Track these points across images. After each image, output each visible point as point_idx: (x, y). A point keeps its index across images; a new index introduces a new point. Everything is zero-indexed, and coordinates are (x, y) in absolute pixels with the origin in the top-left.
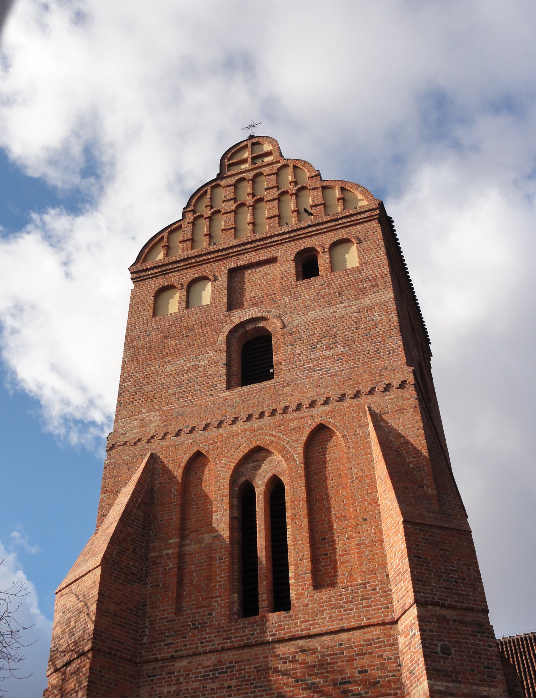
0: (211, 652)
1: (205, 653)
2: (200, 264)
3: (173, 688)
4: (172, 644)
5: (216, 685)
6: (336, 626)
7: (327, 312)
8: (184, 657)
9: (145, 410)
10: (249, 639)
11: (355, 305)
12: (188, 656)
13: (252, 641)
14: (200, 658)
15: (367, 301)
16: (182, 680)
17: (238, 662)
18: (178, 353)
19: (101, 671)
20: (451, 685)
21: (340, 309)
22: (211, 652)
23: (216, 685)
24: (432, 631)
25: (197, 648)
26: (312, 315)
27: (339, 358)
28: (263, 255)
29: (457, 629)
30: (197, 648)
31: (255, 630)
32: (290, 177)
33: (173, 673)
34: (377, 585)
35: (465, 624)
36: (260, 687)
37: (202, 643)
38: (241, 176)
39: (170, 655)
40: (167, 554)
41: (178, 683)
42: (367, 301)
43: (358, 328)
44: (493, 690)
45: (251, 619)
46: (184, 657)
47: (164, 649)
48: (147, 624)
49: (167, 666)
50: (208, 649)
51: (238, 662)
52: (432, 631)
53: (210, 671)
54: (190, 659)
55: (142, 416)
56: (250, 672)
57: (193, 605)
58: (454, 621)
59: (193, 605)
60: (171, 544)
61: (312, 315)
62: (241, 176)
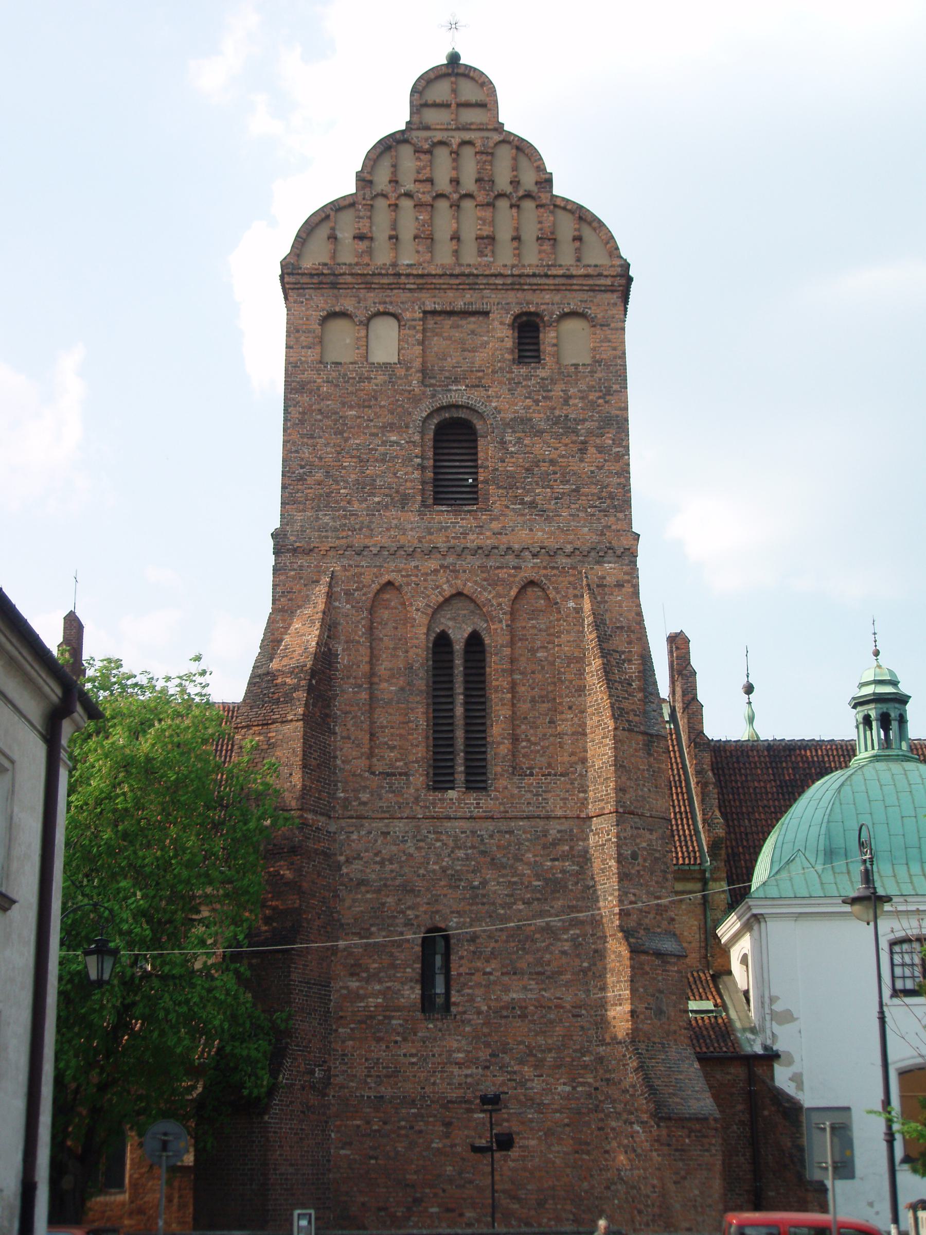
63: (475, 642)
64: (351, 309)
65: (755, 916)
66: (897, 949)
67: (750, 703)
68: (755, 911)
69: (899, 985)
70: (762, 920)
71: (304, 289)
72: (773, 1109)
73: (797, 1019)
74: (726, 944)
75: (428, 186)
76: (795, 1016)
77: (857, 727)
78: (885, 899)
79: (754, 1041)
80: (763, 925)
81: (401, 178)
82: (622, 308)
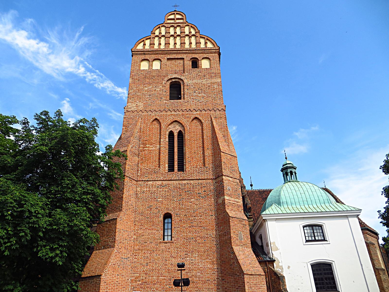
0: (160, 180)
1: (158, 180)
2: (157, 54)
3: (148, 189)
4: (147, 176)
5: (161, 190)
6: (198, 178)
7: (199, 81)
8: (151, 181)
9: (138, 101)
10: (172, 178)
11: (210, 81)
12: (152, 181)
13: (173, 179)
14: (156, 182)
15: (214, 80)
16: (150, 187)
17: (168, 184)
18: (150, 84)
19: (127, 182)
20: (230, 198)
21: (204, 82)
22: (160, 180)
23: (161, 190)
24: (226, 183)
25: (155, 179)
26: (195, 81)
27: (203, 97)
28: (180, 56)
29: (232, 183)
30: (155, 179)
31: (174, 176)
32: (120, 90)
33: (148, 185)
34: (210, 168)
35: (234, 182)
36: (175, 192)
37: (157, 177)
38: (172, 25)
39: (147, 180)
40: (146, 149)
41: (149, 188)
42: (214, 80)
43: (209, 89)
44: (239, 200)
45: (172, 172)
46: (151, 181)
47: (145, 178)
48: (139, 170)
49: (146, 183)
50: (159, 179)
51: (168, 184)
52: (226, 183)
53: (159, 186)
54: (153, 182)
55: (137, 103)
56: (172, 187)
57: (154, 166)
58: (232, 181)
59: (154, 166)
60: (147, 146)
61: (195, 81)
62: (172, 25)
63: (180, 134)
64: (148, 59)
65: (264, 220)
66: (305, 228)
67: (251, 182)
68: (264, 218)
69: (307, 239)
70: (266, 221)
71: (137, 55)
72: (275, 277)
73: (279, 249)
74: (254, 234)
75: (169, 34)
76: (278, 248)
77: (284, 176)
78: (263, 258)
79: (266, 257)
80: (266, 222)
81: (162, 32)
82: (218, 59)
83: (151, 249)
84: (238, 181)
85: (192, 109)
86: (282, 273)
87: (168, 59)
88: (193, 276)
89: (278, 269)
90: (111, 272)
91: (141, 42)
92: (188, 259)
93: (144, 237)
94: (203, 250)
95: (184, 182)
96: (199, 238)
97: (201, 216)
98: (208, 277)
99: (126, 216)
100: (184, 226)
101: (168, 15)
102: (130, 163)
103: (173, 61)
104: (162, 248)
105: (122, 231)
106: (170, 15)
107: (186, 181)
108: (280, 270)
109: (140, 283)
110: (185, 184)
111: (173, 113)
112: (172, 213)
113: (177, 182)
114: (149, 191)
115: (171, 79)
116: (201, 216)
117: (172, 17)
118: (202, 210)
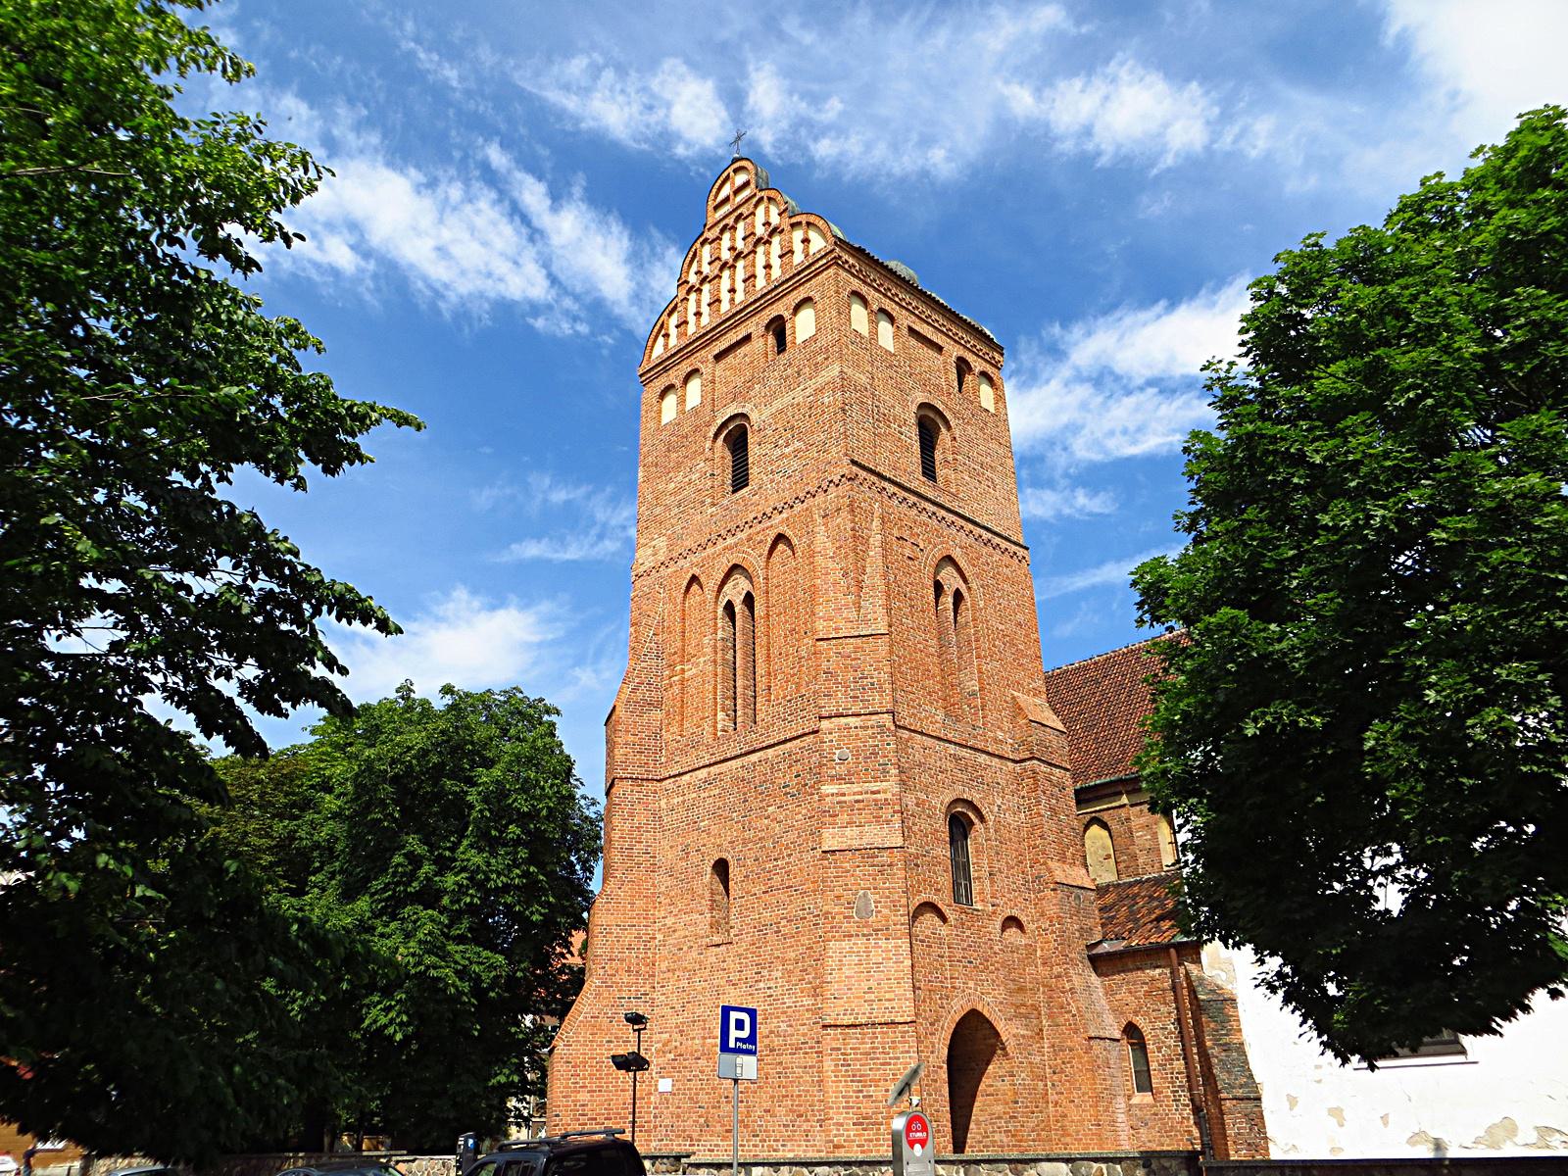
61: (777, 405)
83: (690, 967)
84: (887, 719)
85: (801, 495)
86: (1229, 987)
87: (718, 357)
88: (771, 1032)
89: (1214, 973)
90: (585, 1035)
91: (656, 337)
92: (762, 985)
93: (677, 934)
94: (793, 955)
95: (754, 757)
96: (784, 922)
97: (789, 855)
98: (804, 1035)
99: (625, 888)
100: (753, 891)
101: (712, 197)
102: (631, 738)
103: (730, 359)
104: (710, 960)
105: (616, 930)
106: (719, 189)
107: (758, 754)
108: (1223, 976)
109: (672, 1056)
110: (754, 764)
111: (730, 541)
112: (729, 858)
113: (738, 763)
114: (684, 802)
115: (724, 425)
116: (789, 855)
117: (726, 190)
118: (792, 836)
